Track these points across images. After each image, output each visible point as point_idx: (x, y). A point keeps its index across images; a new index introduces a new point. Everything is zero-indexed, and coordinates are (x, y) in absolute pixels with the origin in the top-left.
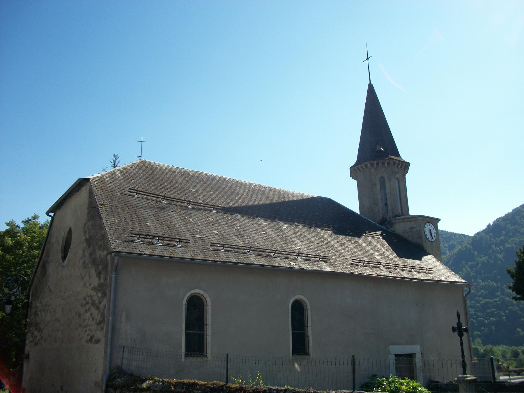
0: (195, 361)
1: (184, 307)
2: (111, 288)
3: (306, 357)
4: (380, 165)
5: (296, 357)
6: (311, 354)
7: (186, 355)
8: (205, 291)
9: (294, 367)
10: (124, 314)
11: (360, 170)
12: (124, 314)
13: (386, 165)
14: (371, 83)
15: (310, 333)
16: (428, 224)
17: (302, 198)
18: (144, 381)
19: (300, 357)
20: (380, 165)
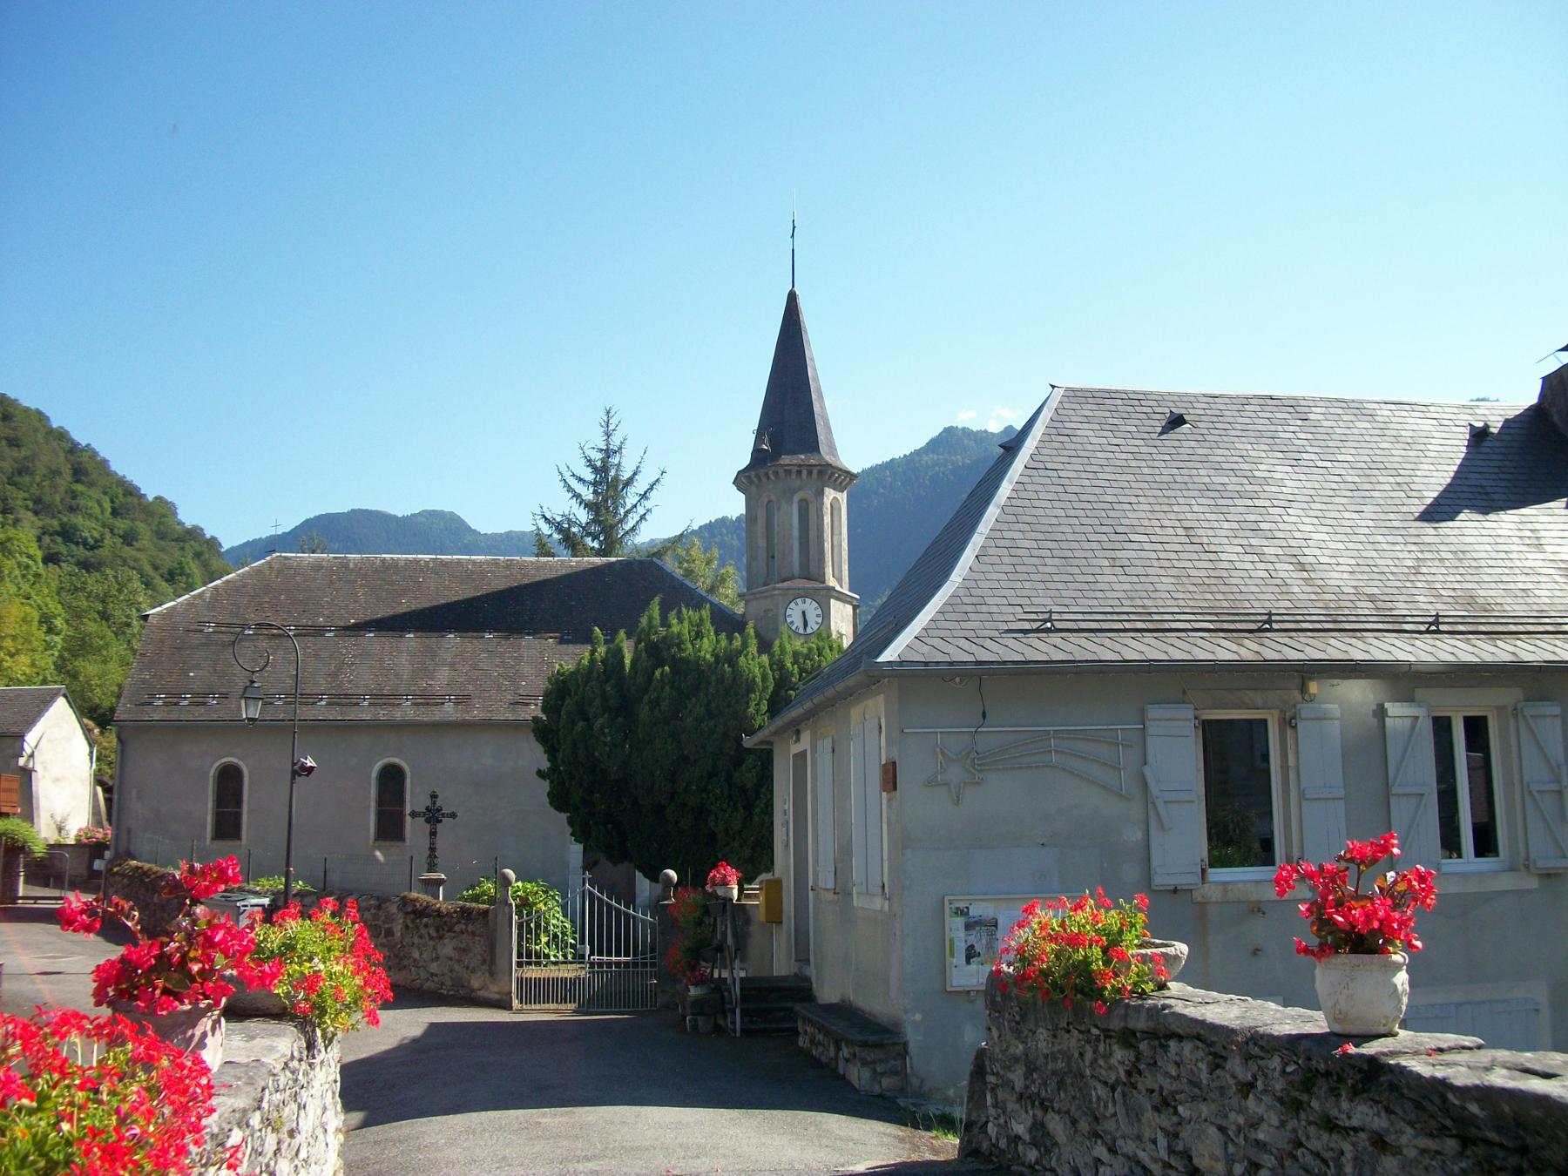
0: (226, 845)
1: (211, 779)
2: (1236, 621)
3: (399, 844)
4: (764, 479)
5: (381, 843)
6: (408, 841)
7: (213, 839)
8: (240, 759)
9: (375, 856)
10: (134, 792)
11: (768, 478)
12: (134, 792)
13: (772, 477)
14: (795, 289)
15: (210, 804)
16: (799, 600)
17: (569, 571)
18: (134, 858)
19: (387, 843)
20: (764, 479)
